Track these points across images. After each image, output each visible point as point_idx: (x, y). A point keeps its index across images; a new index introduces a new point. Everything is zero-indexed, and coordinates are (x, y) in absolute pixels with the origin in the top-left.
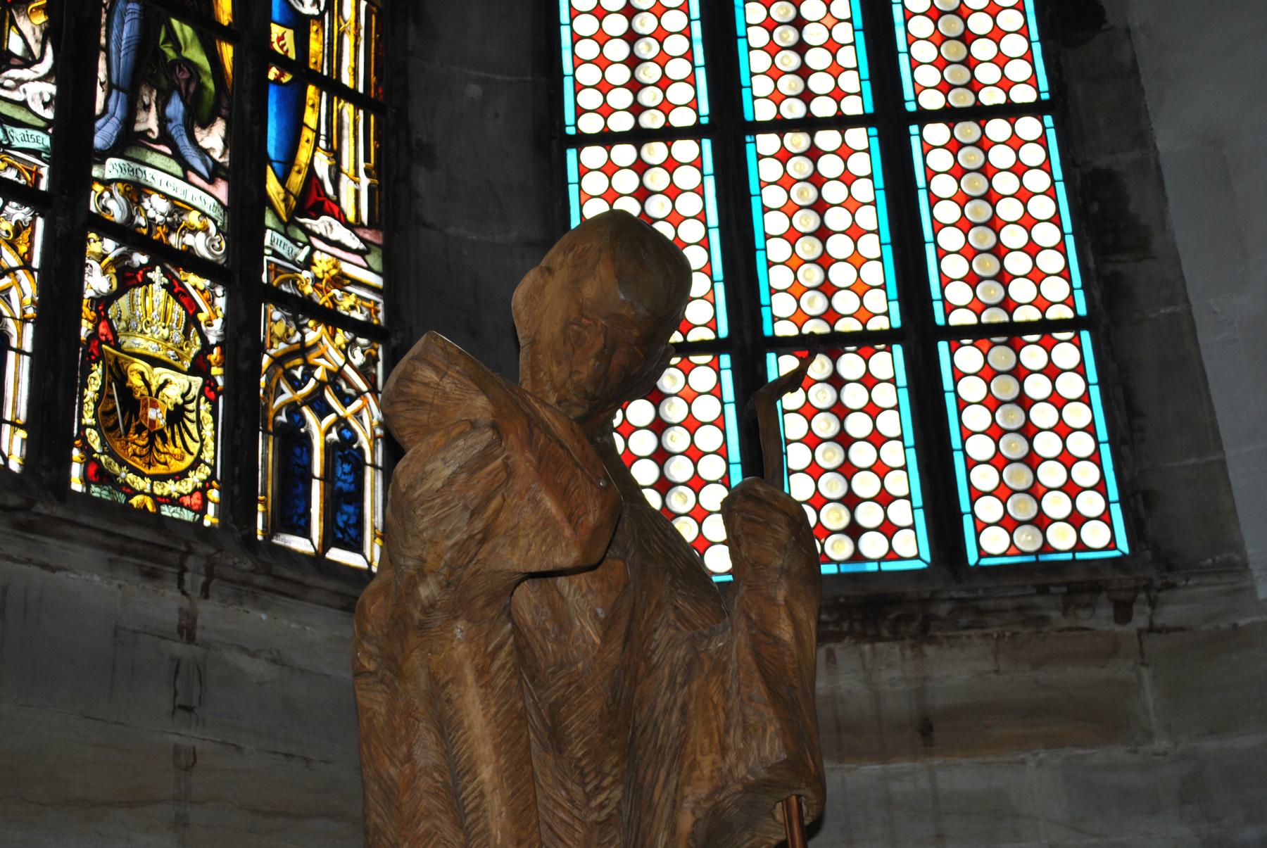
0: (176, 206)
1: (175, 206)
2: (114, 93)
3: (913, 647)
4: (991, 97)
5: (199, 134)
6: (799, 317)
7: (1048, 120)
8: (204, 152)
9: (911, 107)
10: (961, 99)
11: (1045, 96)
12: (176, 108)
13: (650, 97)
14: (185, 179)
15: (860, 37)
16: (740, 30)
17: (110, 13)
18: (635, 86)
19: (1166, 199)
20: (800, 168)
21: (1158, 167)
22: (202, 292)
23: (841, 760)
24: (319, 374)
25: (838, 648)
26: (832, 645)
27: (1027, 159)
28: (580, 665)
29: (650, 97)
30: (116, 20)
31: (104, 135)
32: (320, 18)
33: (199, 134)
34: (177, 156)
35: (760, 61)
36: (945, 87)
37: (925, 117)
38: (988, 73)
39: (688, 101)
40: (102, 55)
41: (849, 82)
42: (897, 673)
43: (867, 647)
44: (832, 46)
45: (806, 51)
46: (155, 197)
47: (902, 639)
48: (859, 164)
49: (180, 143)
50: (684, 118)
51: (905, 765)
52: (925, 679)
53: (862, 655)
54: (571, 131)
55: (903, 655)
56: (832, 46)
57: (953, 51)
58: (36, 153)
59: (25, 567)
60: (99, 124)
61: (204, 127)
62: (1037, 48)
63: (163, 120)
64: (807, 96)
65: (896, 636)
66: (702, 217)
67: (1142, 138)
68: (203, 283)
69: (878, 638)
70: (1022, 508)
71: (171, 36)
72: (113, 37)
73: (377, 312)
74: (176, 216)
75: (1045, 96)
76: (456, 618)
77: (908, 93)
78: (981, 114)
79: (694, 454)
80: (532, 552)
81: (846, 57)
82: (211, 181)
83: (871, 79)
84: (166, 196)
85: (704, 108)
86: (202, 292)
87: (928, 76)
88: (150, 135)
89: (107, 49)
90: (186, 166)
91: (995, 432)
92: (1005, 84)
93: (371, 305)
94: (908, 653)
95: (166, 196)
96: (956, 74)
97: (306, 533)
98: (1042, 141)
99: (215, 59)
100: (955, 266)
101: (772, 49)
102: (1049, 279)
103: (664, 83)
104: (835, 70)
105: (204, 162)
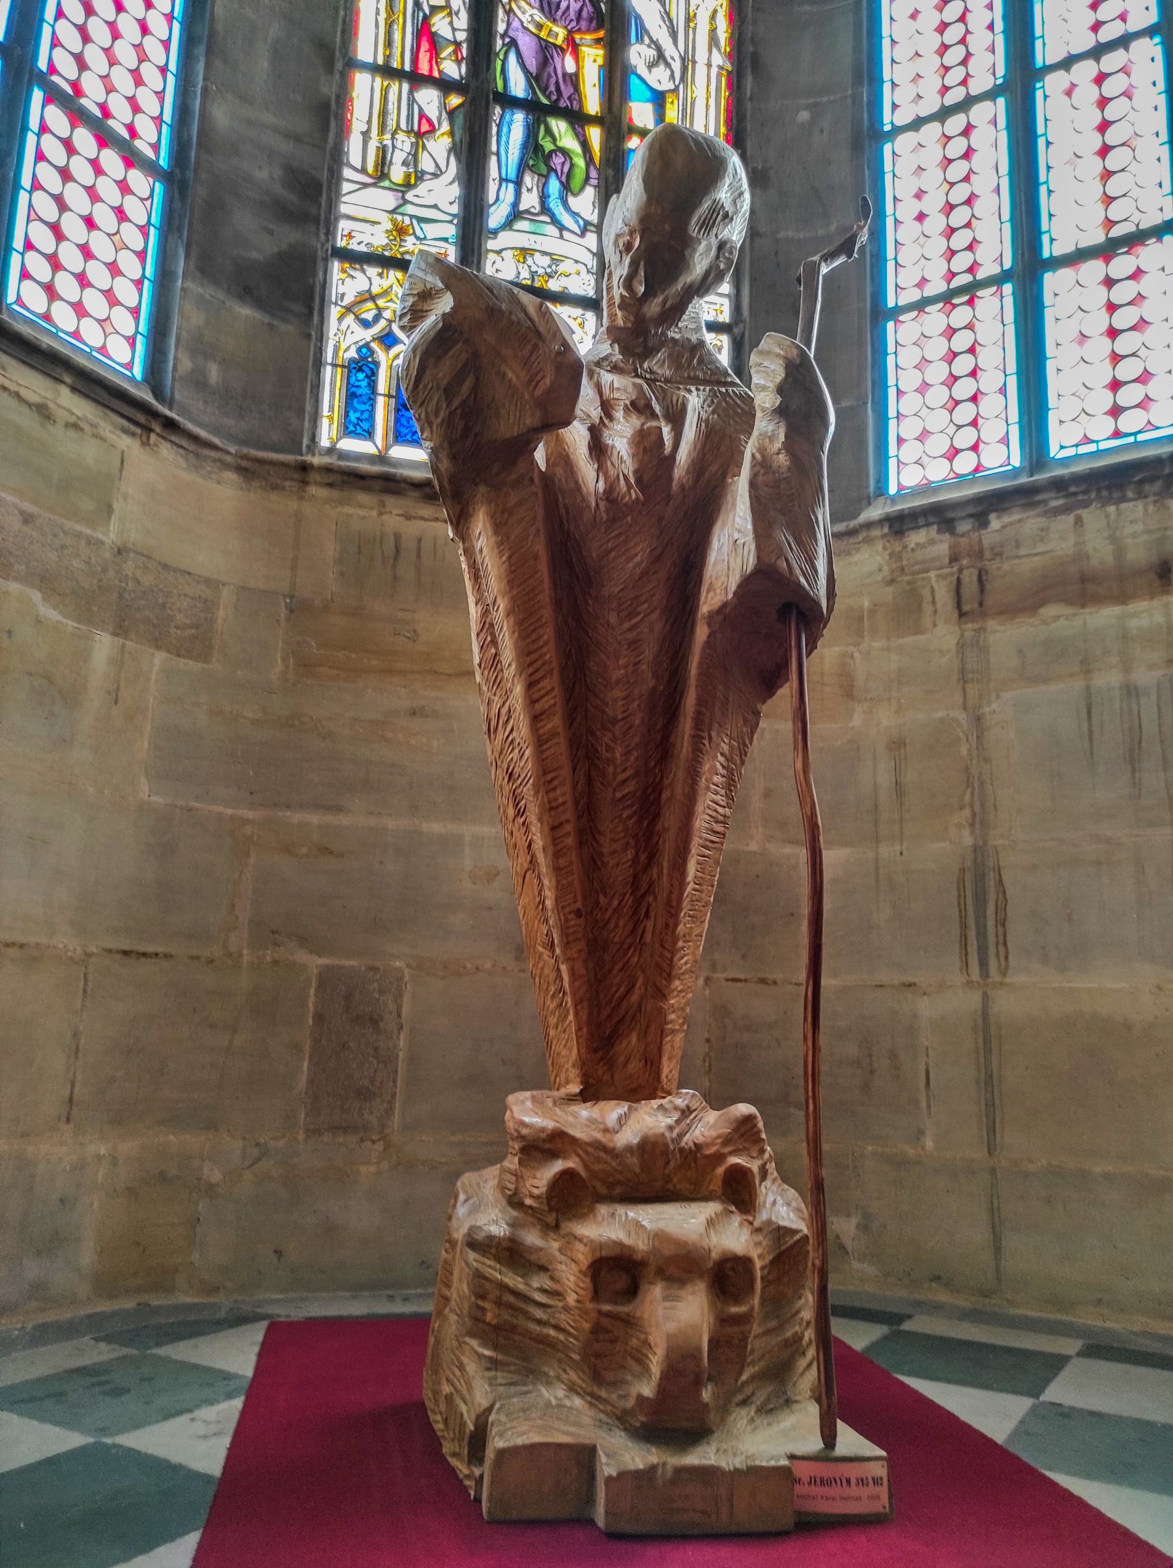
0: (553, 259)
1: (553, 259)
2: (504, 184)
3: (1155, 502)
5: (571, 200)
8: (575, 214)
12: (554, 185)
14: (561, 237)
17: (499, 126)
22: (575, 319)
23: (1083, 606)
24: (387, 314)
25: (1085, 513)
26: (1079, 512)
28: (629, 519)
30: (505, 130)
31: (496, 216)
32: (675, 90)
33: (571, 200)
34: (555, 221)
40: (494, 159)
42: (1139, 527)
43: (1112, 509)
46: (537, 255)
47: (1146, 497)
49: (556, 212)
51: (1142, 605)
52: (1166, 529)
53: (1107, 516)
55: (1146, 510)
58: (446, 240)
59: (434, 524)
60: (492, 210)
61: (575, 195)
63: (544, 198)
65: (1141, 495)
68: (578, 312)
69: (1124, 499)
71: (549, 131)
72: (503, 143)
73: (722, 312)
74: (554, 267)
76: (476, 485)
80: (512, 420)
82: (582, 235)
84: (545, 253)
86: (575, 319)
88: (533, 210)
89: (498, 154)
90: (562, 228)
93: (717, 307)
94: (1151, 508)
95: (545, 253)
97: (369, 434)
99: (585, 145)
105: (577, 222)
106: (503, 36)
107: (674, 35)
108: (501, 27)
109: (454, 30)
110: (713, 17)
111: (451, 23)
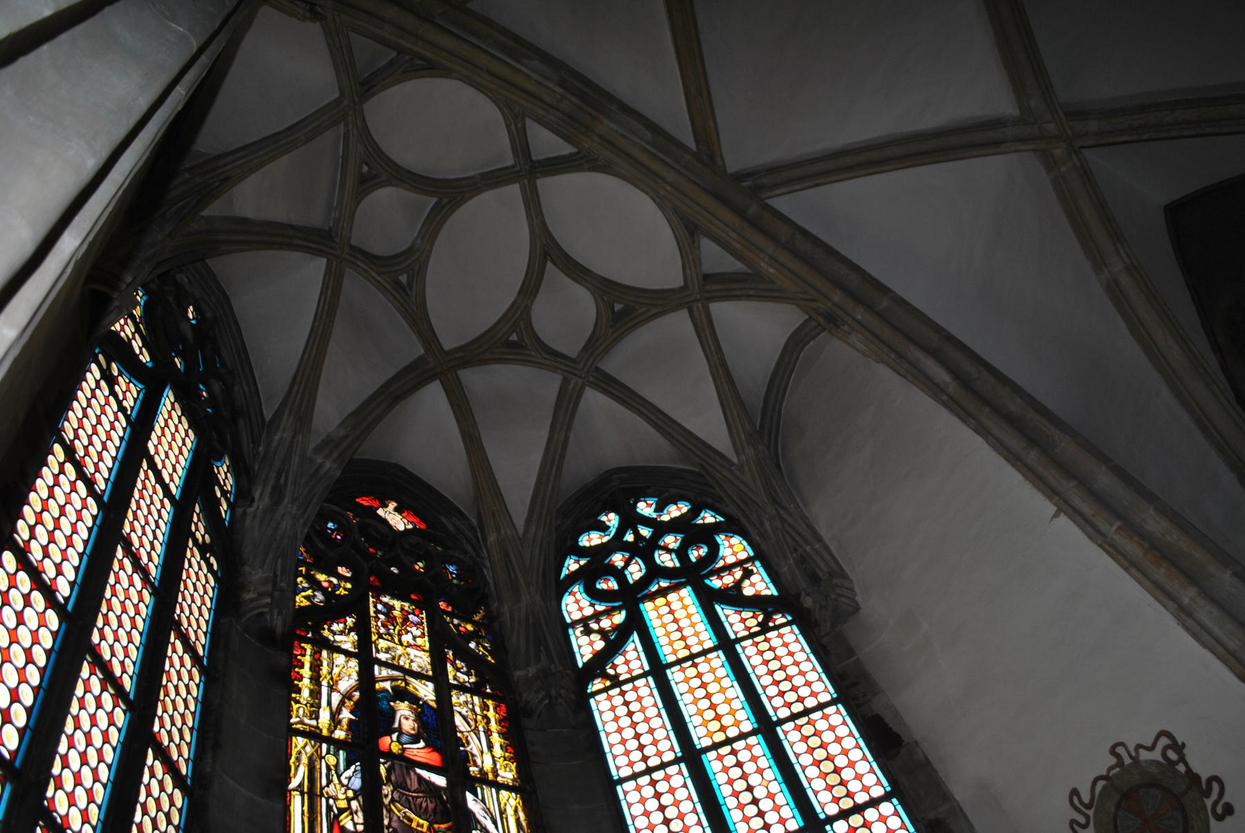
4: (861, 798)
6: (710, 734)
7: (895, 801)
9: (822, 816)
10: (847, 804)
11: (888, 789)
13: (650, 751)
15: (783, 786)
16: (721, 802)
18: (634, 725)
19: (972, 826)
20: (730, 761)
21: (961, 809)
27: (838, 726)
29: (650, 751)
35: (726, 790)
36: (836, 800)
37: (781, 722)
38: (854, 786)
39: (669, 747)
41: (742, 715)
44: (771, 796)
45: (744, 776)
48: (757, 751)
50: (669, 757)
54: (616, 778)
56: (771, 796)
57: (833, 779)
62: (875, 765)
64: (687, 647)
66: (690, 798)
67: (946, 796)
70: (820, 754)
75: (888, 789)
77: (818, 809)
78: (859, 809)
79: (676, 803)
81: (780, 799)
83: (773, 757)
85: (677, 749)
87: (825, 797)
91: (811, 750)
92: (866, 789)
96: (839, 791)
98: (896, 813)
100: (819, 784)
101: (741, 807)
102: (868, 778)
103: (655, 743)
104: (777, 808)
106: (388, 827)
107: (495, 822)
108: (386, 822)
109: (355, 824)
110: (516, 811)
111: (352, 819)
